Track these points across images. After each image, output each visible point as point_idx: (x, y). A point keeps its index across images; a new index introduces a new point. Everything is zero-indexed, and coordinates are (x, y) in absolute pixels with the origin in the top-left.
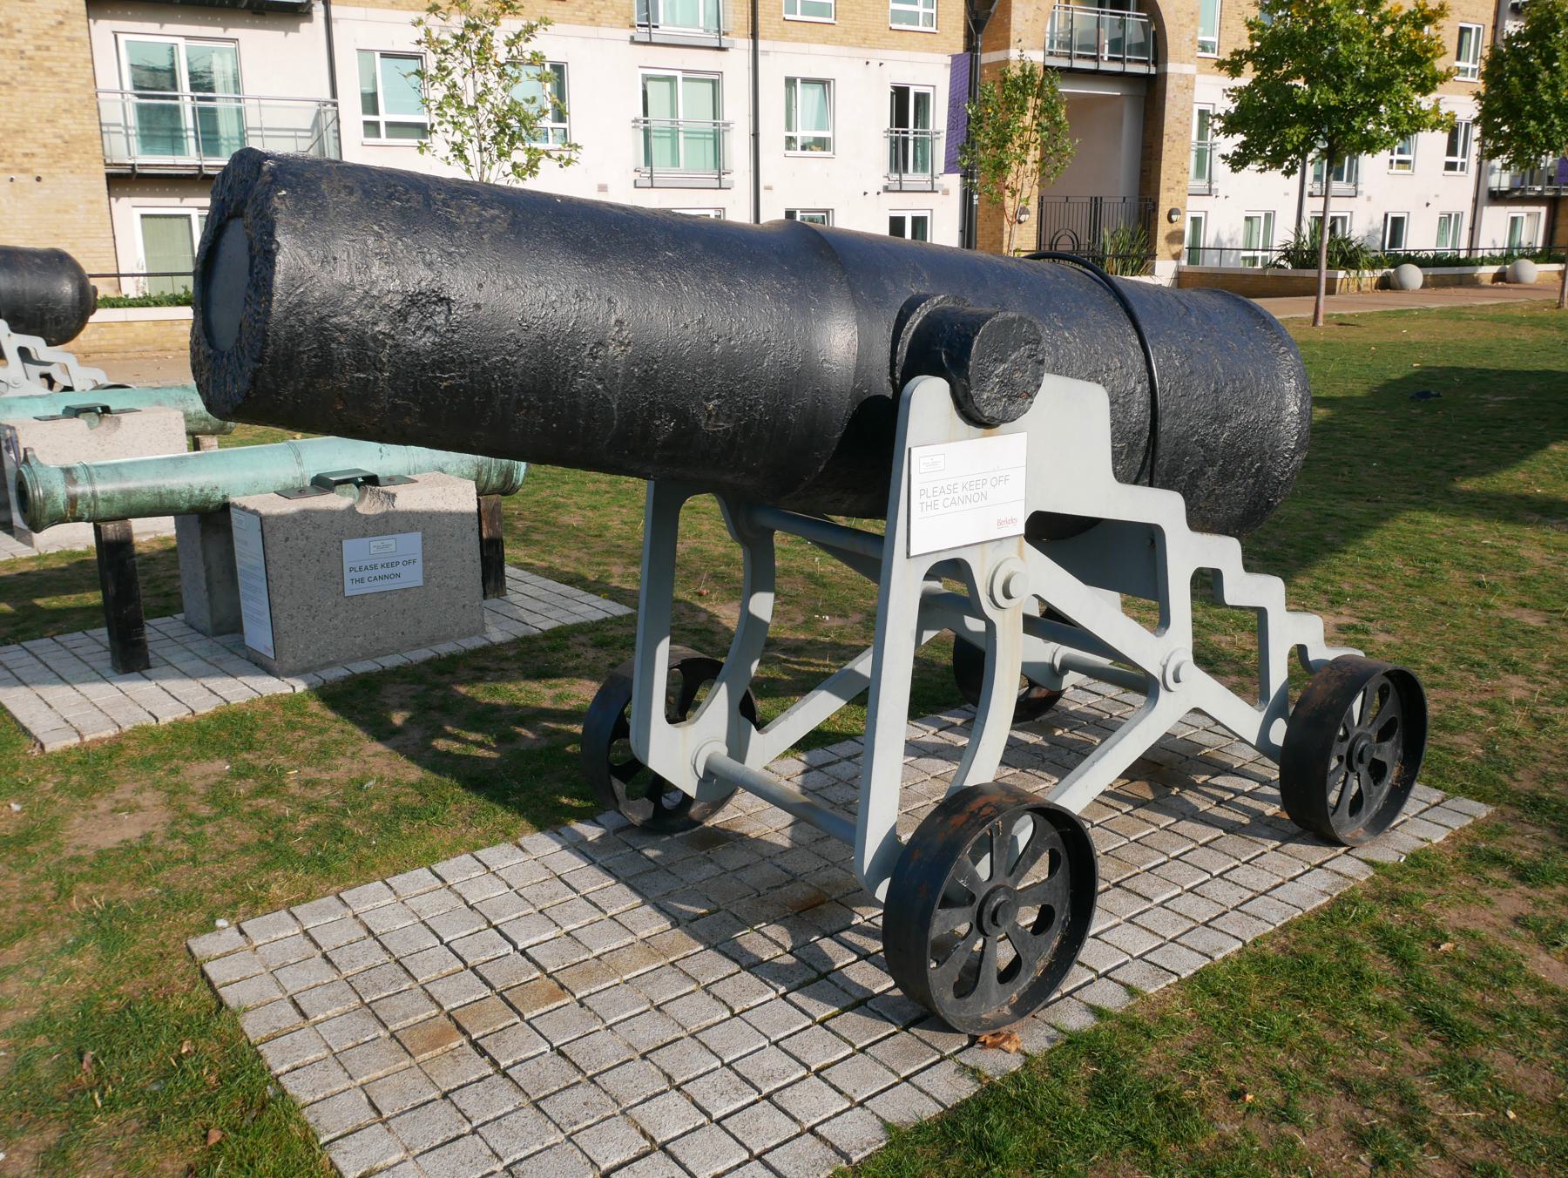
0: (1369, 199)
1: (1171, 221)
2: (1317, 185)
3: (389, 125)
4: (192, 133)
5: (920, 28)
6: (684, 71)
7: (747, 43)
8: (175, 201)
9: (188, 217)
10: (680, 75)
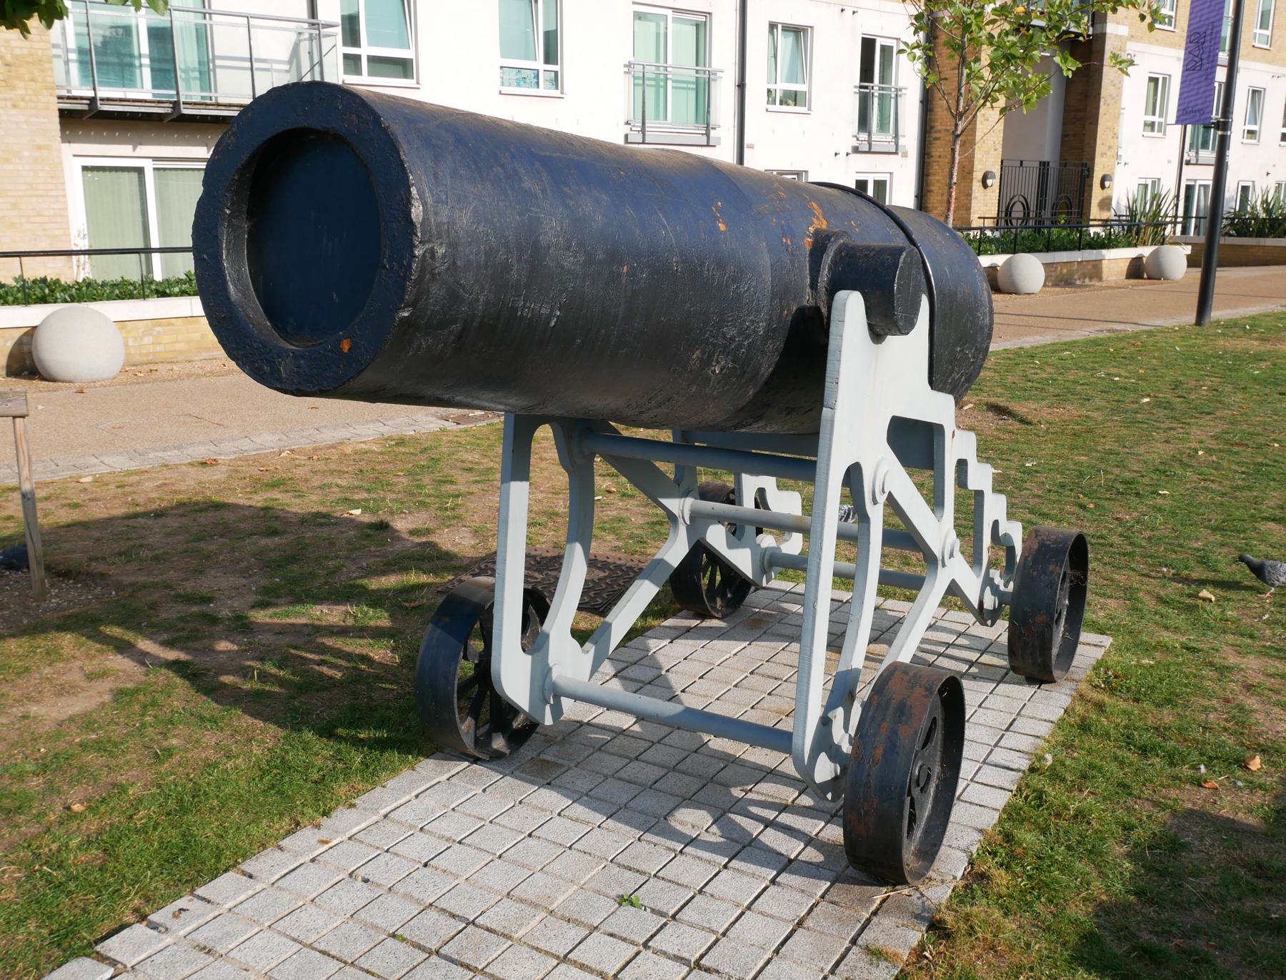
3: (372, 59)
4: (146, 61)
6: (675, 10)
8: (126, 149)
9: (140, 171)
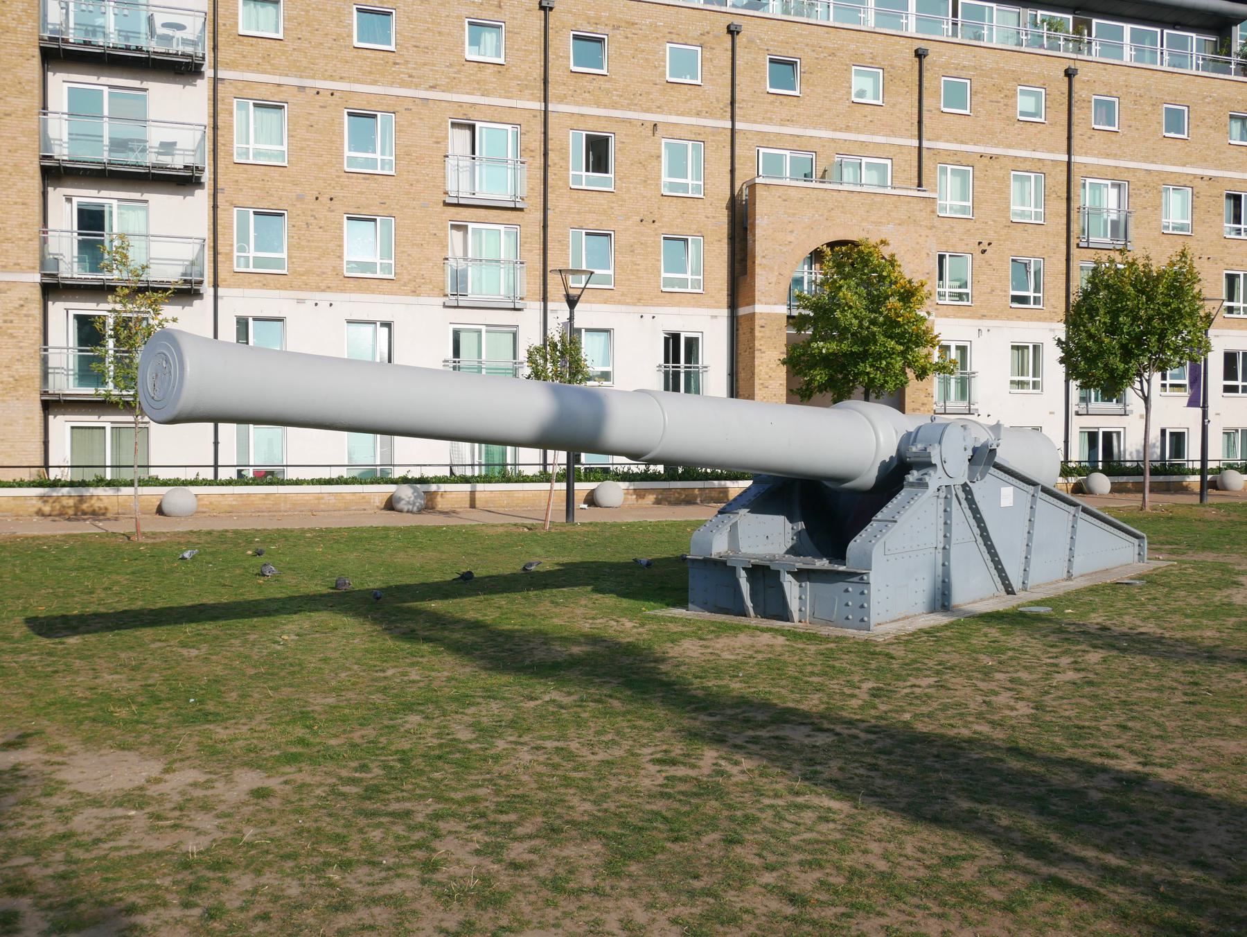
2: (1084, 405)
5: (689, 290)
7: (539, 305)
10: (484, 328)
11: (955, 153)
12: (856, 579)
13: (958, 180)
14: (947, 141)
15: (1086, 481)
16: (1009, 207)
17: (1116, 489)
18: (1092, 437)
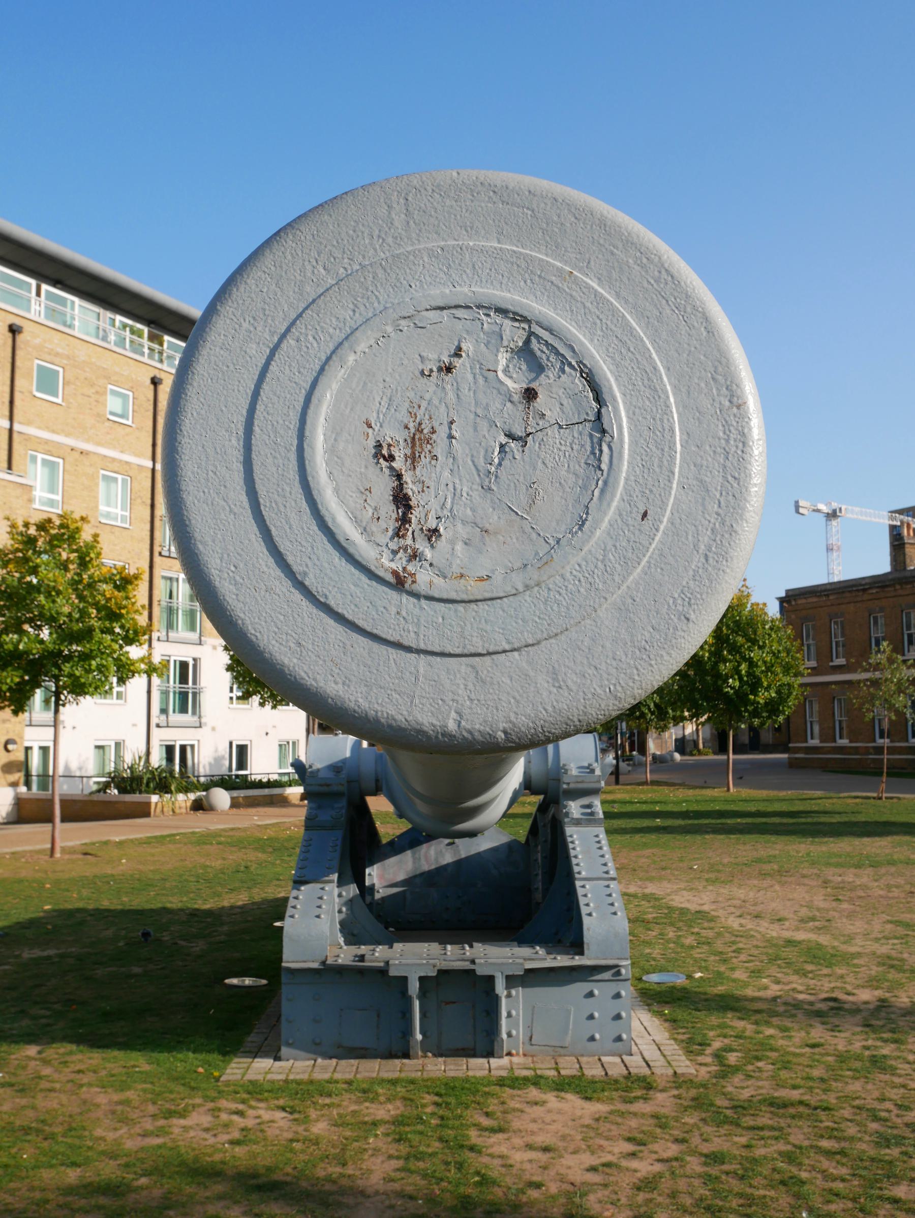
0: (213, 729)
1: (7, 750)
2: (163, 717)
11: (47, 442)
12: (607, 975)
13: (46, 470)
14: (39, 428)
15: (207, 797)
16: (97, 507)
17: (235, 804)
18: (170, 750)
